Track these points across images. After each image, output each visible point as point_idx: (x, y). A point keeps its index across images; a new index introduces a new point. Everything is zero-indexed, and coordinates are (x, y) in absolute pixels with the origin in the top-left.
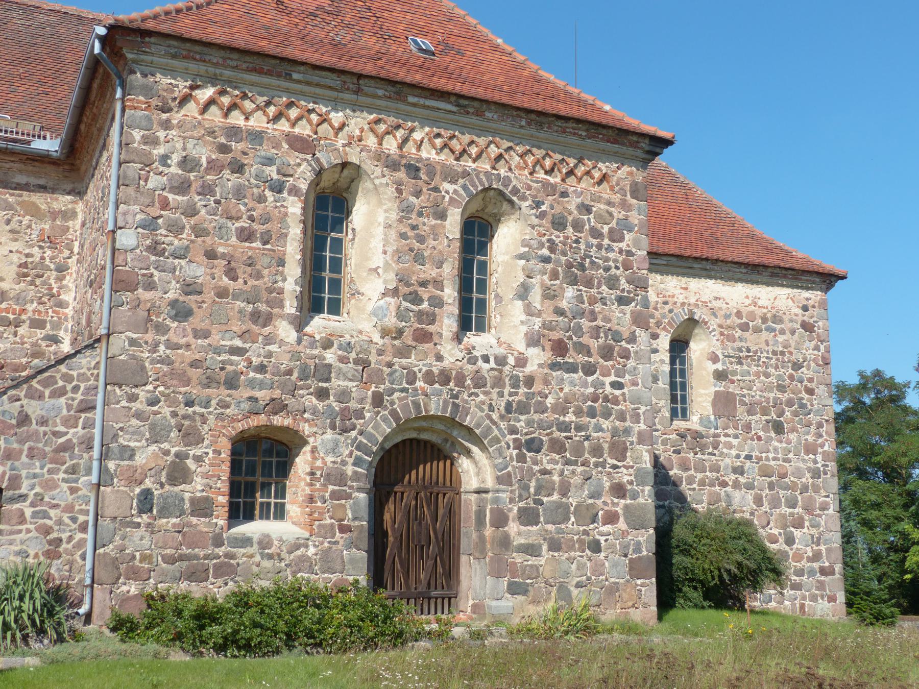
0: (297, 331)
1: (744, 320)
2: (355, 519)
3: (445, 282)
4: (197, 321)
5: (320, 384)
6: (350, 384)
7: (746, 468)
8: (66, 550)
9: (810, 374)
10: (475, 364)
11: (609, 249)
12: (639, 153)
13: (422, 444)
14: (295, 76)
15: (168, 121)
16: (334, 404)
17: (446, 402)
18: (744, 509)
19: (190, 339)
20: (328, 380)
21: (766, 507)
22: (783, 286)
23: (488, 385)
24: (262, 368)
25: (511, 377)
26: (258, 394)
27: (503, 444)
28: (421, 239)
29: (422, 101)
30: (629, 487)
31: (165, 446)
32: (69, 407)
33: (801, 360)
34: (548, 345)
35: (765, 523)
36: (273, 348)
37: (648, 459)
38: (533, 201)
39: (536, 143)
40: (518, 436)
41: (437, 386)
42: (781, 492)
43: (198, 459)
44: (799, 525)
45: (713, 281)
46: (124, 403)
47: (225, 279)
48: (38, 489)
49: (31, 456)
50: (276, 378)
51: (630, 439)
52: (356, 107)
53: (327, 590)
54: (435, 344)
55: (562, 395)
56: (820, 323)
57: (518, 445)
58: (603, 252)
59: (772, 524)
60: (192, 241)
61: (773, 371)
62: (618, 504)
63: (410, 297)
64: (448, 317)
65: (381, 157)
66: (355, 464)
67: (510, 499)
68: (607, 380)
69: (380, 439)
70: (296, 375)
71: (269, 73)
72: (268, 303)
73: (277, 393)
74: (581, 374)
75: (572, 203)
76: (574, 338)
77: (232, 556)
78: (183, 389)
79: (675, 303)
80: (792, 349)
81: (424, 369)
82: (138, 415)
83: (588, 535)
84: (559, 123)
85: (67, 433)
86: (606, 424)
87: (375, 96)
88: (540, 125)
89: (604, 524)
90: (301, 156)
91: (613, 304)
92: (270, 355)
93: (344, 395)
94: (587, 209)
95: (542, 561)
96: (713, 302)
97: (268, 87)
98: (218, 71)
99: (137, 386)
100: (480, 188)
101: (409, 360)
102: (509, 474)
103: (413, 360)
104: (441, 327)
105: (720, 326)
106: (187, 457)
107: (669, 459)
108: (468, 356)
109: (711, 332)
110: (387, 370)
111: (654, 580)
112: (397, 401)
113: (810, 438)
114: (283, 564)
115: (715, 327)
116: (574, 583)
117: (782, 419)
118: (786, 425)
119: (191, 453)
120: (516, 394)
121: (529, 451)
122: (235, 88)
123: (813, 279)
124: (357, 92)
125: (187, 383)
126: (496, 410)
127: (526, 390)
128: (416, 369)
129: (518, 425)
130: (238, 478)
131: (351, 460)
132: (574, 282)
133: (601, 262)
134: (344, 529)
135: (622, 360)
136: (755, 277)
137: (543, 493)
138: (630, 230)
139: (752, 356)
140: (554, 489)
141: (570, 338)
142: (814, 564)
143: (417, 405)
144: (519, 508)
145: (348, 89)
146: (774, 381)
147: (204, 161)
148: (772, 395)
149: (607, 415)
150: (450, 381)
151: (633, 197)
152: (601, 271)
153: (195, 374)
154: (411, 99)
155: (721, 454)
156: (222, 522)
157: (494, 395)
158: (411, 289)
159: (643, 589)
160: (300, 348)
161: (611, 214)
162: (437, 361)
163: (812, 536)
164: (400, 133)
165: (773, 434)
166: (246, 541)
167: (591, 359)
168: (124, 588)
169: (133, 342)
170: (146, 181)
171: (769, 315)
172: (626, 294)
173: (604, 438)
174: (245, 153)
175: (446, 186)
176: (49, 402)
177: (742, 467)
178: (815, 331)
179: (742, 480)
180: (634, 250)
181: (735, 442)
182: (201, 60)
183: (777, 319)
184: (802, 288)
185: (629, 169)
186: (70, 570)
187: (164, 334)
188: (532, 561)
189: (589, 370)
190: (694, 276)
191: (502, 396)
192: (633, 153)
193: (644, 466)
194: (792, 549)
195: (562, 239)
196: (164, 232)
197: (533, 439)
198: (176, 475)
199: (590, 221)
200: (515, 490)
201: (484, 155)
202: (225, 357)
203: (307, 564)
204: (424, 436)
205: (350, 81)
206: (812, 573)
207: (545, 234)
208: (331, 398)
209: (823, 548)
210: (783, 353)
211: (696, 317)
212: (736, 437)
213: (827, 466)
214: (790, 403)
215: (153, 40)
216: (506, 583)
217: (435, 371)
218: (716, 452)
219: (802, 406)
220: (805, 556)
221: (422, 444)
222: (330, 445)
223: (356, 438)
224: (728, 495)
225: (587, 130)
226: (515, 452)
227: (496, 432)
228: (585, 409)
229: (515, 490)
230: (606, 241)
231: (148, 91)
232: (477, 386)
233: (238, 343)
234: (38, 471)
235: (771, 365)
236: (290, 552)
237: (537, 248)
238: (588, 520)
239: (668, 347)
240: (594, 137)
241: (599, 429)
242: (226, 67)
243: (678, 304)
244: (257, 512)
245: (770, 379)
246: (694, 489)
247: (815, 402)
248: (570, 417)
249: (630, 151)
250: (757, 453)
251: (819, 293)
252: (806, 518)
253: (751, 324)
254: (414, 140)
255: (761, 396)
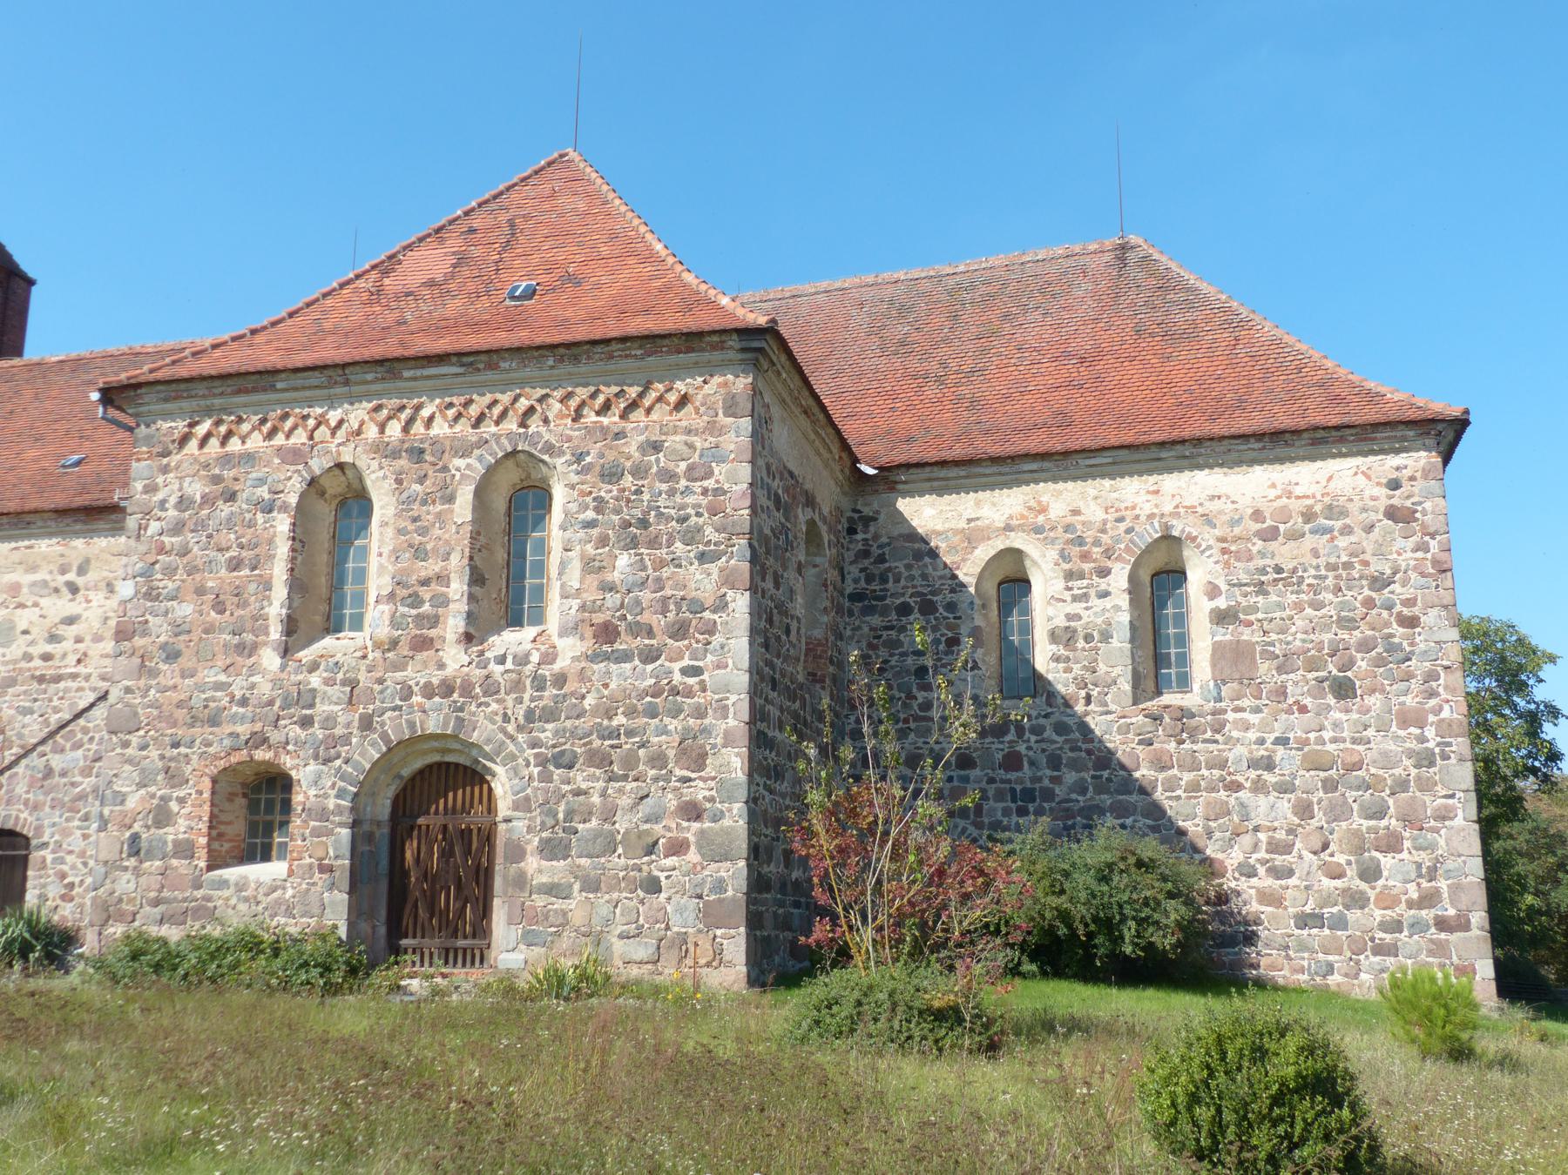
0: (283, 657)
1: (1269, 523)
2: (337, 857)
3: (452, 575)
4: (186, 661)
5: (304, 712)
6: (336, 708)
7: (1277, 759)
8: (78, 894)
9: (1408, 593)
10: (485, 667)
11: (687, 491)
12: (731, 355)
13: (461, 769)
14: (279, 385)
15: (168, 465)
16: (318, 732)
17: (447, 717)
18: (1276, 824)
19: (178, 680)
20: (312, 706)
21: (1319, 818)
22: (1341, 455)
23: (503, 691)
24: (244, 702)
25: (535, 678)
26: (239, 729)
27: (520, 760)
28: (423, 532)
29: (419, 373)
30: (708, 805)
31: (153, 789)
32: (85, 757)
33: (1388, 572)
34: (589, 632)
35: (1318, 846)
36: (256, 679)
37: (739, 765)
38: (573, 455)
39: (582, 381)
40: (543, 750)
41: (437, 699)
42: (1351, 795)
43: (182, 801)
44: (1392, 844)
45: (1207, 471)
46: (118, 750)
47: (213, 614)
48: (57, 837)
49: (53, 807)
50: (258, 710)
51: (712, 741)
52: (353, 399)
53: (1405, 974)
54: (437, 650)
55: (606, 692)
56: (1428, 505)
57: (542, 762)
58: (678, 498)
59: (1333, 847)
60: (183, 581)
61: (1330, 596)
62: (688, 829)
63: (409, 600)
64: (454, 616)
65: (384, 451)
66: (337, 797)
67: (529, 827)
68: (677, 666)
69: (368, 766)
70: (278, 704)
71: (255, 390)
72: (253, 631)
73: (258, 727)
74: (637, 662)
75: (632, 446)
76: (629, 617)
77: (208, 899)
78: (169, 732)
79: (1137, 517)
80: (1367, 557)
81: (422, 681)
82: (129, 761)
83: (640, 870)
84: (599, 349)
85: (82, 783)
86: (673, 724)
87: (366, 382)
88: (576, 359)
89: (666, 856)
90: (292, 468)
91: (691, 564)
92: (253, 686)
93: (329, 722)
94: (656, 447)
95: (571, 904)
96: (1207, 504)
97: (260, 404)
98: (208, 402)
99: (130, 733)
100: (500, 454)
101: (405, 673)
102: (527, 799)
103: (409, 672)
104: (445, 630)
105: (1222, 540)
106: (170, 799)
107: (1132, 753)
108: (477, 659)
109: (1203, 552)
110: (377, 688)
111: (742, 930)
112: (388, 722)
113: (1410, 701)
114: (260, 908)
115: (1211, 542)
116: (617, 932)
117: (1349, 674)
118: (1358, 683)
119: (175, 795)
120: (541, 698)
121: (558, 766)
122: (230, 414)
123: (1399, 434)
124: (347, 383)
125: (174, 725)
126: (513, 720)
127: (555, 692)
128: (410, 683)
129: (542, 736)
130: (257, 818)
131: (333, 793)
132: (633, 543)
133: (673, 512)
134: (323, 869)
135: (701, 637)
136: (1281, 451)
137: (576, 818)
138: (722, 460)
139: (1286, 577)
140: (590, 813)
141: (624, 617)
142: (1424, 913)
143: (411, 725)
144: (541, 839)
145: (336, 383)
146: (1333, 613)
147: (198, 498)
148: (1327, 637)
149: (676, 712)
150: (453, 692)
151: (726, 415)
152: (674, 523)
153: (181, 714)
154: (406, 374)
155: (1228, 740)
156: (202, 864)
157: (510, 703)
158: (410, 591)
159: (725, 942)
160: (284, 675)
161: (691, 446)
162: (439, 669)
163: (1419, 866)
164: (404, 416)
165: (1331, 700)
166: (223, 884)
167: (653, 642)
168: (111, 930)
169: (128, 690)
170: (146, 529)
171: (1318, 508)
172: (712, 547)
173: (668, 743)
174: (236, 479)
175: (459, 462)
176: (71, 755)
177: (1269, 757)
178: (1416, 520)
179: (1270, 778)
180: (726, 486)
181: (1254, 719)
182: (188, 397)
183: (1332, 511)
184: (1382, 451)
185: (721, 379)
186: (81, 913)
187: (155, 678)
188: (559, 904)
189: (650, 656)
190: (1170, 470)
191: (521, 703)
192: (721, 357)
193: (733, 775)
194: (1373, 888)
195: (615, 493)
196: (159, 576)
197: (563, 753)
198: (160, 817)
199: (657, 461)
200: (535, 817)
201: (511, 413)
202: (208, 694)
203: (283, 908)
204: (449, 758)
205: (336, 375)
206: (1417, 927)
207: (591, 493)
208: (316, 725)
209: (1443, 884)
210: (1348, 566)
211: (1175, 533)
212: (1257, 710)
213: (1449, 744)
214: (1366, 646)
215: (143, 390)
216: (520, 931)
217: (435, 681)
218: (1218, 737)
219: (1392, 649)
220: (1404, 898)
221: (461, 769)
222: (312, 778)
223: (340, 767)
224: (1242, 805)
225: (640, 347)
226: (536, 770)
227: (512, 747)
228: (640, 708)
229: (535, 817)
230: (683, 483)
231: (148, 440)
232: (486, 693)
233: (223, 678)
234: (57, 820)
235: (1326, 588)
236: (267, 895)
237: (577, 512)
238: (640, 852)
239: (1125, 585)
240: (656, 352)
241: (664, 731)
242: (215, 395)
243: (1143, 518)
244: (274, 853)
245: (1324, 611)
246: (1178, 798)
247: (1418, 639)
248: (620, 720)
249: (716, 356)
250: (1299, 734)
251: (1423, 454)
252: (1406, 834)
253: (1282, 527)
254: (422, 418)
255: (1304, 641)
